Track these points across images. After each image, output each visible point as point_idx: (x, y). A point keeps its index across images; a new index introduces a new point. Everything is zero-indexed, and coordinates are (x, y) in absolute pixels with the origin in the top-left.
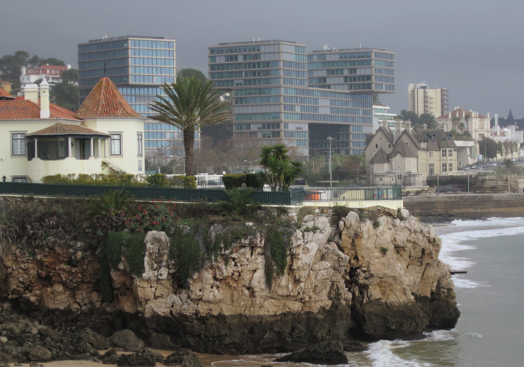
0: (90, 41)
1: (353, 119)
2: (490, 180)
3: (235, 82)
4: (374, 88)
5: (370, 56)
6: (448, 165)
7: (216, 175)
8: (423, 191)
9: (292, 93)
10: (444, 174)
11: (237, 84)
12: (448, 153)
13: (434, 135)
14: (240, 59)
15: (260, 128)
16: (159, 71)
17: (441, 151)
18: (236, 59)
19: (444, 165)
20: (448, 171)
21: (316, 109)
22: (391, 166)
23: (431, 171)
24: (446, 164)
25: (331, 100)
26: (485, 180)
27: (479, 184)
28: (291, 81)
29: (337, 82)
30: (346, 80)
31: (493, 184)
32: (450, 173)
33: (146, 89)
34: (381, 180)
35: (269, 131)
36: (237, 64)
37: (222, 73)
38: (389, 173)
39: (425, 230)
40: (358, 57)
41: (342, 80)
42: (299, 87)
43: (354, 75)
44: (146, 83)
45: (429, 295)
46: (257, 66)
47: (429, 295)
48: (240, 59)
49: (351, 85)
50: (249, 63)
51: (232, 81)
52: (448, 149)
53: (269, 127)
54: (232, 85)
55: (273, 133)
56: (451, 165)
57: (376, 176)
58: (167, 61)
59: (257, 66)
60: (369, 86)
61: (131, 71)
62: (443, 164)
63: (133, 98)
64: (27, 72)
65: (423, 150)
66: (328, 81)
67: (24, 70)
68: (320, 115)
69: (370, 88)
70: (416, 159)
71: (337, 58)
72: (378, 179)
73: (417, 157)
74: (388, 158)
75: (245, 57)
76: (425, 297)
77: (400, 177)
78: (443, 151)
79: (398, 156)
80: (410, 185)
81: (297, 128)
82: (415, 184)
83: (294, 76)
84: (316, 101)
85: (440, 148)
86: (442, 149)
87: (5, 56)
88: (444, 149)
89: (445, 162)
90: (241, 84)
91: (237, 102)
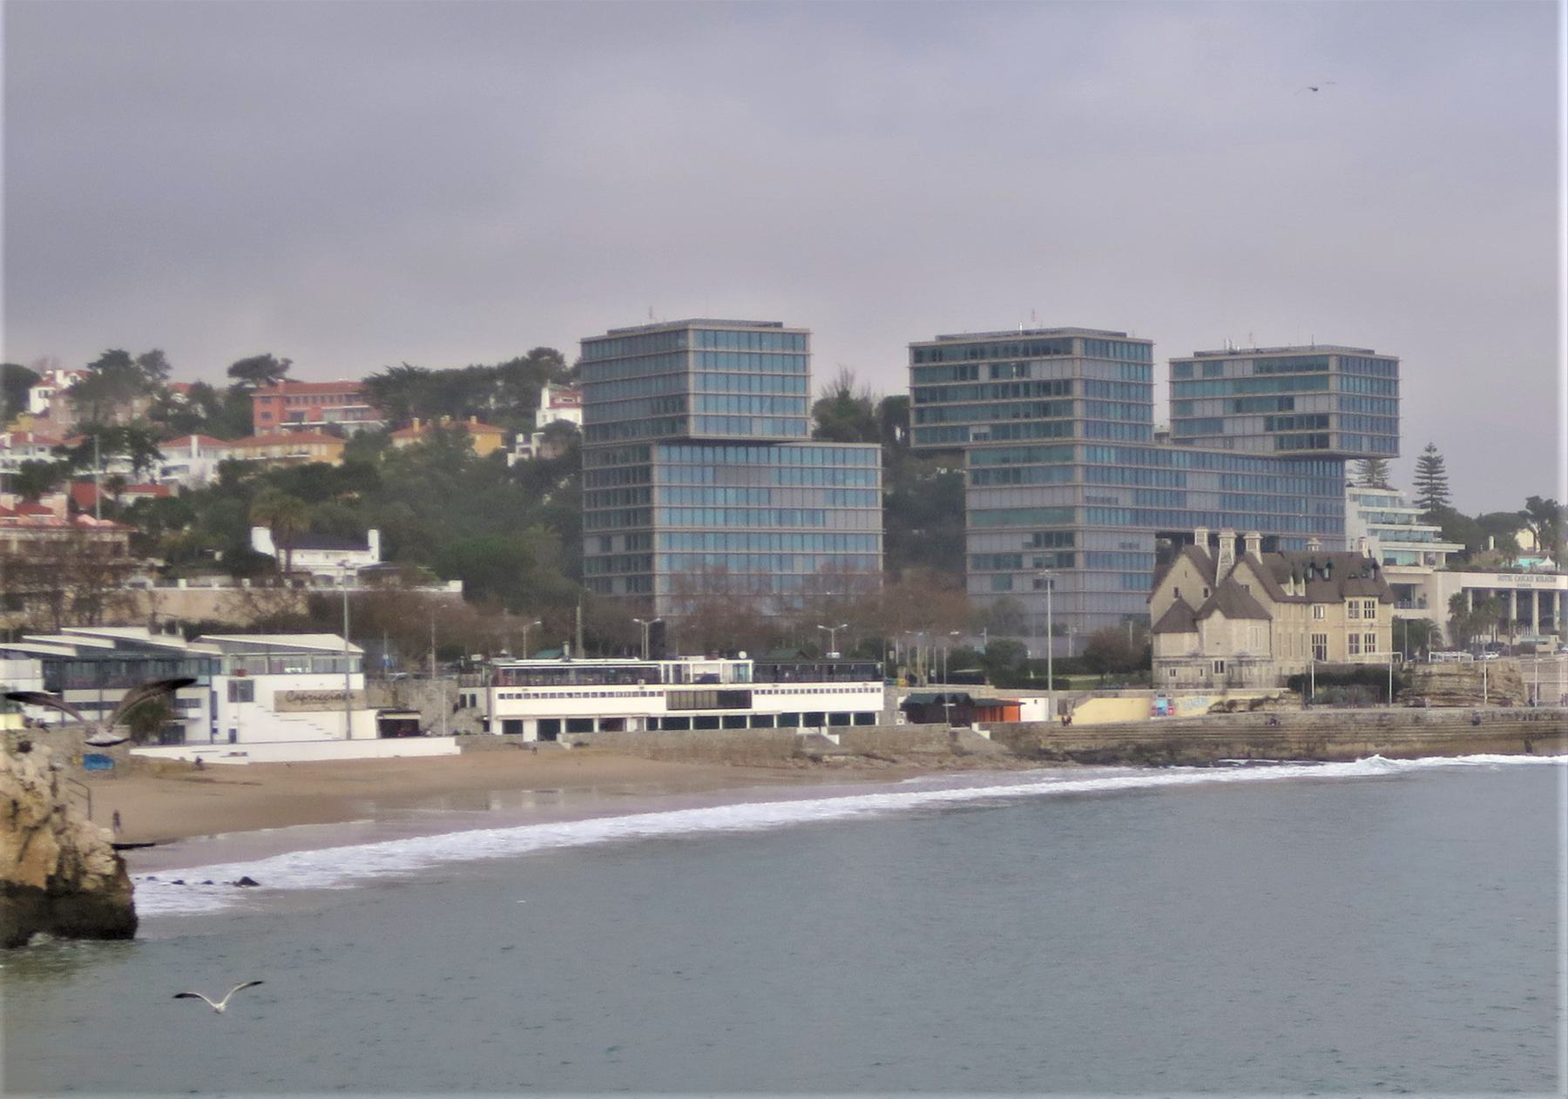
0: (611, 332)
1: (1287, 522)
2: (1441, 675)
3: (973, 431)
4: (1334, 446)
5: (1326, 367)
6: (1362, 639)
7: (722, 661)
8: (1267, 699)
9: (1110, 459)
10: (1351, 659)
11: (976, 437)
12: (1362, 610)
13: (1329, 566)
14: (984, 376)
15: (1028, 545)
16: (767, 403)
17: (1346, 605)
18: (975, 375)
19: (1354, 639)
20: (1362, 653)
21: (1180, 496)
22: (1201, 640)
23: (1320, 653)
24: (1357, 636)
25: (1224, 476)
26: (1430, 675)
27: (1416, 683)
28: (1106, 428)
29: (1249, 431)
30: (1269, 427)
31: (1448, 684)
32: (1368, 659)
33: (719, 450)
34: (1173, 673)
35: (1048, 552)
36: (976, 387)
37: (941, 409)
38: (1195, 655)
39: (16, 766)
40: (1300, 369)
41: (1260, 426)
42: (1128, 442)
43: (1289, 413)
44: (734, 436)
45: (42, 885)
46: (1022, 389)
47: (42, 885)
48: (984, 376)
49: (1281, 438)
50: (1005, 386)
51: (965, 429)
52: (1362, 601)
53: (1049, 542)
54: (965, 438)
55: (1060, 555)
56: (1370, 638)
57: (1161, 663)
58: (789, 381)
59: (1022, 389)
60: (1323, 441)
61: (694, 405)
62: (1351, 637)
63: (709, 472)
64: (552, 400)
65: (1295, 600)
66: (1229, 428)
67: (546, 396)
68: (1191, 513)
69: (1327, 446)
70: (1266, 623)
71: (1248, 371)
72: (1165, 671)
73: (1270, 619)
74: (1194, 621)
75: (995, 372)
76: (34, 890)
77: (1220, 667)
78: (1350, 605)
79: (1217, 616)
80: (1241, 685)
81: (1123, 546)
82: (1251, 683)
83: (1115, 416)
84: (1179, 476)
85: (1342, 597)
86: (1348, 600)
87: (392, 371)
88: (1353, 599)
89: (1354, 632)
90: (985, 436)
91: (976, 482)
